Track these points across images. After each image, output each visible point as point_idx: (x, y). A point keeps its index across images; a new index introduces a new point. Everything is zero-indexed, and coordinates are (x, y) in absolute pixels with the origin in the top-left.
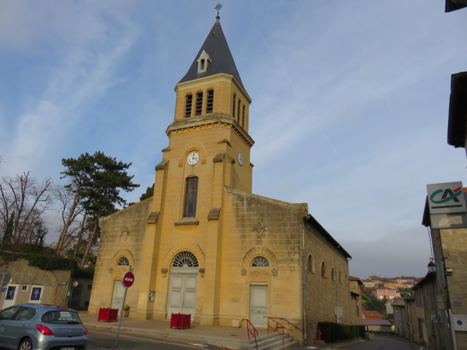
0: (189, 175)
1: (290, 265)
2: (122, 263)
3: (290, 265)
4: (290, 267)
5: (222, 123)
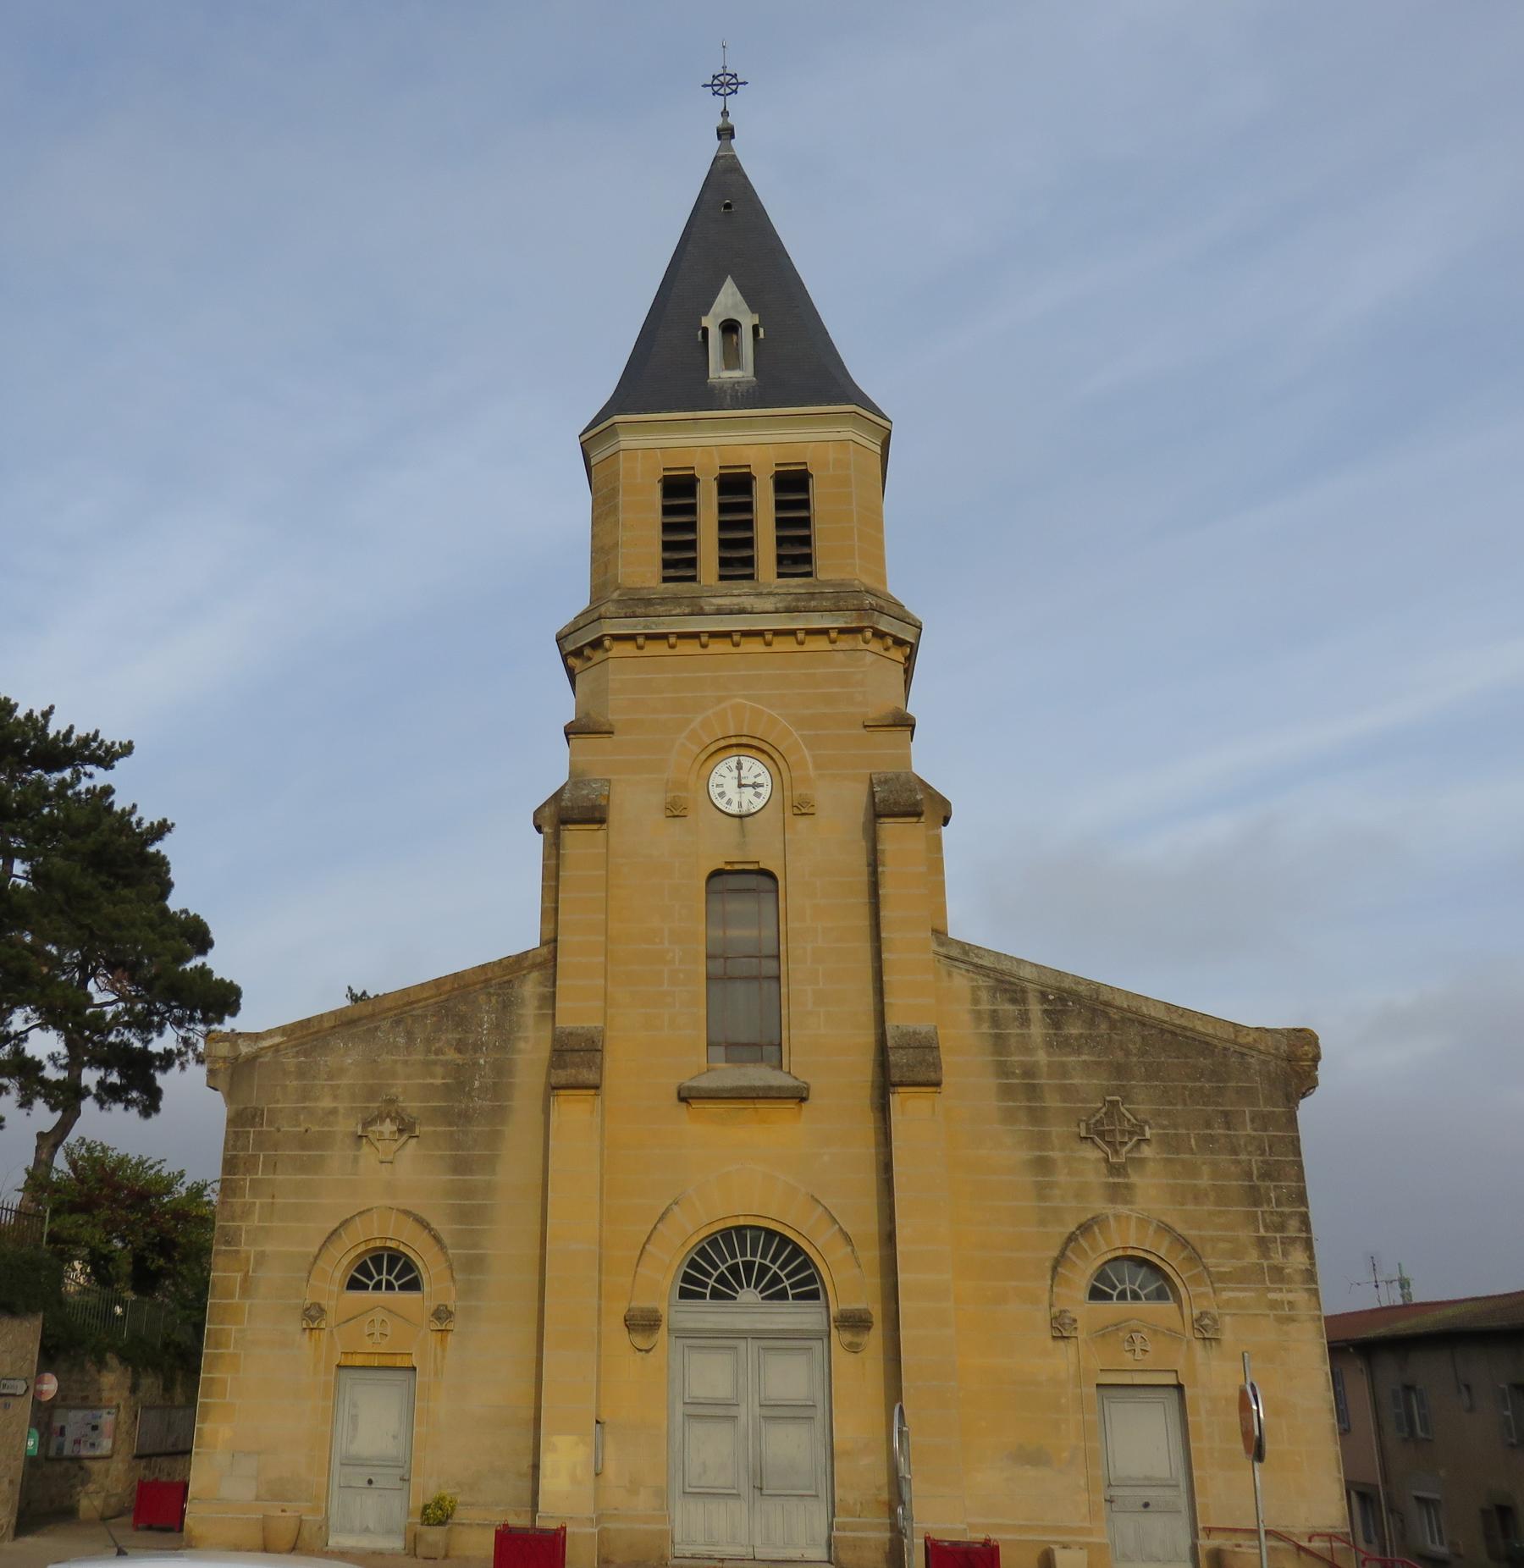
0: (727, 863)
1: (1271, 1296)
2: (371, 1278)
3: (1271, 1296)
4: (1274, 1305)
5: (879, 635)
